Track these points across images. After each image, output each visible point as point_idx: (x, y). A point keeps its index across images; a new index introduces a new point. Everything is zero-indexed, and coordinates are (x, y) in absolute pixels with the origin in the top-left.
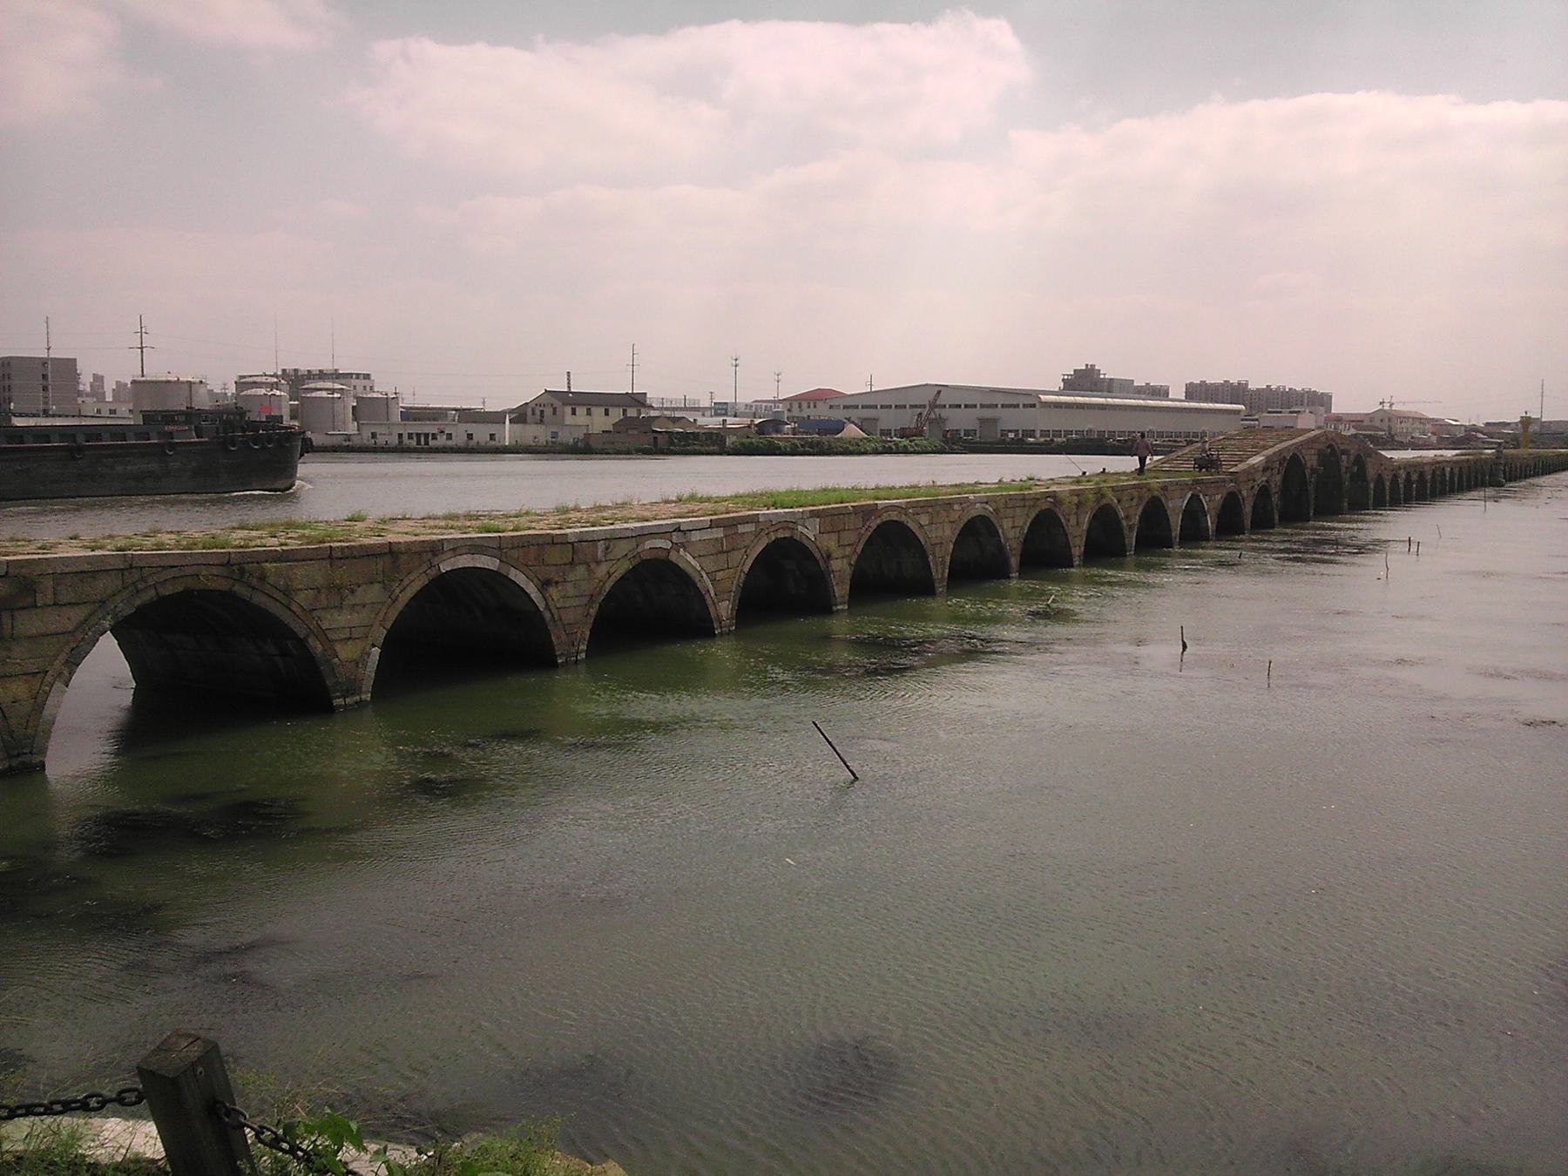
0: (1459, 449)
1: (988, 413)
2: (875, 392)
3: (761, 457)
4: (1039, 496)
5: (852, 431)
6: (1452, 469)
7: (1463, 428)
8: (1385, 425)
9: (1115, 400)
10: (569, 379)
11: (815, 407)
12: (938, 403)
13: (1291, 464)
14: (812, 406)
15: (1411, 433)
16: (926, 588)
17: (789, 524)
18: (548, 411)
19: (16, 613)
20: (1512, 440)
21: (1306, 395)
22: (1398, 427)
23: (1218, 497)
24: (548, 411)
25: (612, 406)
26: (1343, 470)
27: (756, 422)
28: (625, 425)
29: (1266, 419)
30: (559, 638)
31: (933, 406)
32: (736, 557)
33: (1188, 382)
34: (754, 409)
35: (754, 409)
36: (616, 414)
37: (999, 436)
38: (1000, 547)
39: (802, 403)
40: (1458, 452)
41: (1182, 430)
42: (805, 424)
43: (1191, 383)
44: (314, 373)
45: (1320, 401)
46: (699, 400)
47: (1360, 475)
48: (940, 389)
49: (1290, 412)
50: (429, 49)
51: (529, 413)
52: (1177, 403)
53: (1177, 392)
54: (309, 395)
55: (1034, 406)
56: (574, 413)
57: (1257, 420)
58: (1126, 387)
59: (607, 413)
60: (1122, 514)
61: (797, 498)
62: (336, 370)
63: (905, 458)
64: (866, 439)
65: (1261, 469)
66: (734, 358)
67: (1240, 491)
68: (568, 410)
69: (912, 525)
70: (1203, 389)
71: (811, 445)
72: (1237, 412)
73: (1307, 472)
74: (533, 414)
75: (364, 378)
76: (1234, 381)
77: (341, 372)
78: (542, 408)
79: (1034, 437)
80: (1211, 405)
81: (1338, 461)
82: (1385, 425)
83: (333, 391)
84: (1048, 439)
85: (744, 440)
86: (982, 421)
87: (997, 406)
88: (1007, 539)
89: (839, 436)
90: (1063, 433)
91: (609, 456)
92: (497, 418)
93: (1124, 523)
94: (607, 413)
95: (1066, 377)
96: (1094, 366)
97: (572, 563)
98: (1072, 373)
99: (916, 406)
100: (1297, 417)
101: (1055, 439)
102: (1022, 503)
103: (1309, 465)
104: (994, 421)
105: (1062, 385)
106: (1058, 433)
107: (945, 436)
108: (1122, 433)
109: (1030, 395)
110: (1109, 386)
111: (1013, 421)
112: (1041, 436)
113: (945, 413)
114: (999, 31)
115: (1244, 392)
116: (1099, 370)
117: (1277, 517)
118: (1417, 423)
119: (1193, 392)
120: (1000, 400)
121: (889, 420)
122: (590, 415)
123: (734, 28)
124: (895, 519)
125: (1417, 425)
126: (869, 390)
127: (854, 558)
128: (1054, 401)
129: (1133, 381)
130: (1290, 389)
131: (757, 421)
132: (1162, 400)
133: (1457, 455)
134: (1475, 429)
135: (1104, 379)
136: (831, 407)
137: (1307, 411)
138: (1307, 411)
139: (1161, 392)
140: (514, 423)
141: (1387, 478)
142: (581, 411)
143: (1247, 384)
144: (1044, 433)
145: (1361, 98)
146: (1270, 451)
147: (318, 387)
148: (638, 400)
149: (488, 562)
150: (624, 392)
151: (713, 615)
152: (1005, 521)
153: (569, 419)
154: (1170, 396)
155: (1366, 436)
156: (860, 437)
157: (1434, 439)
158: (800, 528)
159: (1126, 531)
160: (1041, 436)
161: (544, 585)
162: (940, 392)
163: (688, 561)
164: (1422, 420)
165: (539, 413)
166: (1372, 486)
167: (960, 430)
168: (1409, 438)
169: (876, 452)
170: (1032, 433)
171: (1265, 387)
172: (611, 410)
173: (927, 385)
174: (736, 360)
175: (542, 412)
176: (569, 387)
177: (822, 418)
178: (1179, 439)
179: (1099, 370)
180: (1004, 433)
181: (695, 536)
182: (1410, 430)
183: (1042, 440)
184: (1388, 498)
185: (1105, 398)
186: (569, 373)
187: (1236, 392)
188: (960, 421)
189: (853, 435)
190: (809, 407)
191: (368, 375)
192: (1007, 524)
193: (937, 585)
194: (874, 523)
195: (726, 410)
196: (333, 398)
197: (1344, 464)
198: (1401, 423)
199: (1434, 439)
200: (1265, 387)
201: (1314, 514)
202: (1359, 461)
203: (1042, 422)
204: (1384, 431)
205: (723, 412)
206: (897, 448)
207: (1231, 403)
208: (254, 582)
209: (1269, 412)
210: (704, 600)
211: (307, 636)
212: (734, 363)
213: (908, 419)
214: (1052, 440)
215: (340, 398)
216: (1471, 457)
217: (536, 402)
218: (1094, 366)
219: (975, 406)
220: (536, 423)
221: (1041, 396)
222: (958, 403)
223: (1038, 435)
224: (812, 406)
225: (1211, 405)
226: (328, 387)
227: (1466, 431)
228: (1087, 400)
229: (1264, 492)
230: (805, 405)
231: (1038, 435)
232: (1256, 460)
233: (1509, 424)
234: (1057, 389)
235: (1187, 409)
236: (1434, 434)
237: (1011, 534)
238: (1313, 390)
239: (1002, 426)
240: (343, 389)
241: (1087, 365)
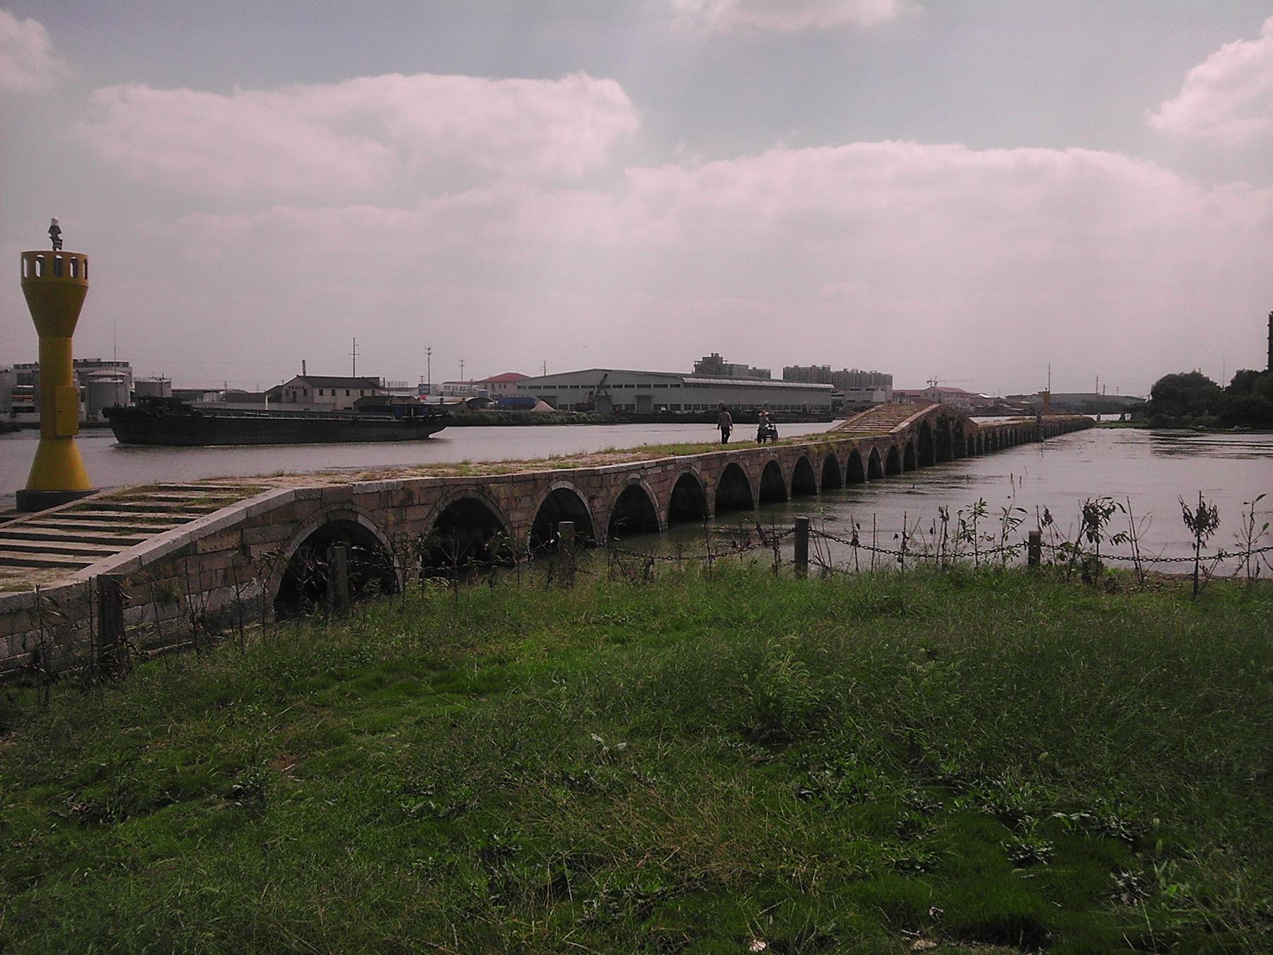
0: (1009, 416)
1: (643, 392)
2: (548, 376)
3: (507, 427)
4: (799, 448)
5: (543, 406)
6: (1011, 430)
7: (992, 400)
9: (739, 381)
10: (304, 367)
11: (505, 387)
12: (605, 384)
13: (922, 427)
14: (502, 387)
15: (955, 404)
16: (749, 507)
17: (688, 465)
18: (300, 393)
19: (407, 509)
20: (1030, 409)
21: (873, 376)
23: (886, 449)
24: (300, 393)
25: (325, 387)
26: (951, 431)
27: (467, 400)
28: (365, 406)
30: (596, 530)
31: (602, 386)
32: (667, 483)
33: (785, 366)
34: (451, 388)
35: (451, 388)
36: (355, 395)
37: (652, 409)
38: (782, 480)
39: (495, 384)
40: (1009, 418)
42: (504, 402)
43: (787, 367)
44: (79, 361)
45: (885, 380)
46: (407, 382)
47: (960, 435)
48: (606, 373)
49: (867, 390)
50: (145, 93)
51: (284, 392)
53: (777, 375)
54: (96, 381)
55: (679, 386)
56: (321, 394)
57: (842, 396)
59: (348, 394)
60: (839, 460)
61: (685, 449)
62: (98, 359)
63: (573, 427)
64: (553, 412)
65: (907, 430)
66: (427, 347)
67: (898, 445)
68: (317, 391)
69: (742, 467)
71: (514, 417)
72: (829, 389)
73: (932, 432)
74: (287, 394)
75: (124, 366)
76: (819, 365)
77: (102, 361)
78: (294, 390)
79: (680, 410)
80: (809, 385)
81: (947, 424)
83: (116, 377)
84: (690, 411)
85: (461, 414)
86: (639, 398)
87: (650, 386)
88: (785, 475)
89: (533, 410)
90: (569, 406)
92: (258, 398)
93: (840, 465)
94: (348, 394)
95: (697, 363)
96: (718, 354)
97: (601, 487)
98: (701, 360)
99: (586, 387)
100: (872, 394)
101: (695, 411)
102: (792, 453)
103: (932, 428)
104: (648, 398)
105: (694, 370)
107: (614, 409)
109: (676, 377)
110: (730, 370)
111: (664, 398)
112: (685, 409)
113: (611, 391)
114: (610, 88)
116: (722, 358)
117: (916, 462)
119: (789, 374)
120: (653, 382)
121: (565, 398)
122: (322, 395)
123: (396, 80)
124: (734, 462)
125: (959, 398)
126: (543, 375)
127: (717, 485)
128: (694, 382)
129: (748, 366)
130: (861, 372)
131: (468, 399)
133: (1008, 420)
134: (999, 400)
135: (726, 364)
136: (519, 387)
137: (880, 389)
138: (880, 389)
139: (765, 375)
140: (273, 402)
141: (975, 436)
142: (327, 392)
143: (829, 368)
144: (688, 407)
145: (888, 146)
146: (911, 419)
147: (102, 374)
148: (372, 383)
149: (569, 485)
150: (361, 377)
151: (658, 519)
152: (784, 463)
153: (317, 399)
154: (772, 378)
156: (550, 411)
157: (972, 409)
158: (693, 467)
159: (841, 471)
160: (685, 409)
161: (591, 499)
162: (606, 375)
163: (647, 485)
164: (963, 395)
165: (292, 393)
166: (967, 442)
167: (567, 406)
169: (562, 423)
170: (678, 407)
171: (842, 370)
172: (351, 391)
173: (594, 370)
174: (429, 349)
175: (294, 392)
176: (304, 373)
177: (517, 396)
179: (722, 358)
180: (658, 407)
181: (650, 472)
182: (954, 402)
183: (686, 412)
184: (976, 450)
186: (304, 361)
187: (822, 374)
188: (623, 398)
189: (543, 409)
190: (500, 387)
191: (127, 363)
192: (785, 465)
193: (754, 504)
194: (725, 464)
195: (429, 390)
196: (117, 383)
197: (951, 427)
198: (948, 397)
199: (972, 409)
200: (842, 370)
201: (937, 461)
202: (959, 425)
203: (685, 398)
205: (426, 391)
206: (579, 419)
208: (486, 494)
209: (851, 390)
210: (654, 510)
211: (505, 525)
212: (427, 351)
213: (581, 397)
214: (693, 412)
215: (121, 383)
216: (1021, 422)
217: (289, 385)
218: (718, 354)
219: (633, 386)
220: (290, 402)
221: (684, 378)
222: (620, 384)
223: (683, 409)
224: (502, 387)
226: (111, 374)
227: (995, 402)
228: (718, 381)
229: (909, 446)
230: (497, 385)
231: (683, 409)
232: (904, 424)
234: (690, 373)
235: (792, 387)
236: (971, 405)
237: (787, 472)
238: (879, 372)
239: (656, 401)
240: (123, 376)
241: (712, 354)
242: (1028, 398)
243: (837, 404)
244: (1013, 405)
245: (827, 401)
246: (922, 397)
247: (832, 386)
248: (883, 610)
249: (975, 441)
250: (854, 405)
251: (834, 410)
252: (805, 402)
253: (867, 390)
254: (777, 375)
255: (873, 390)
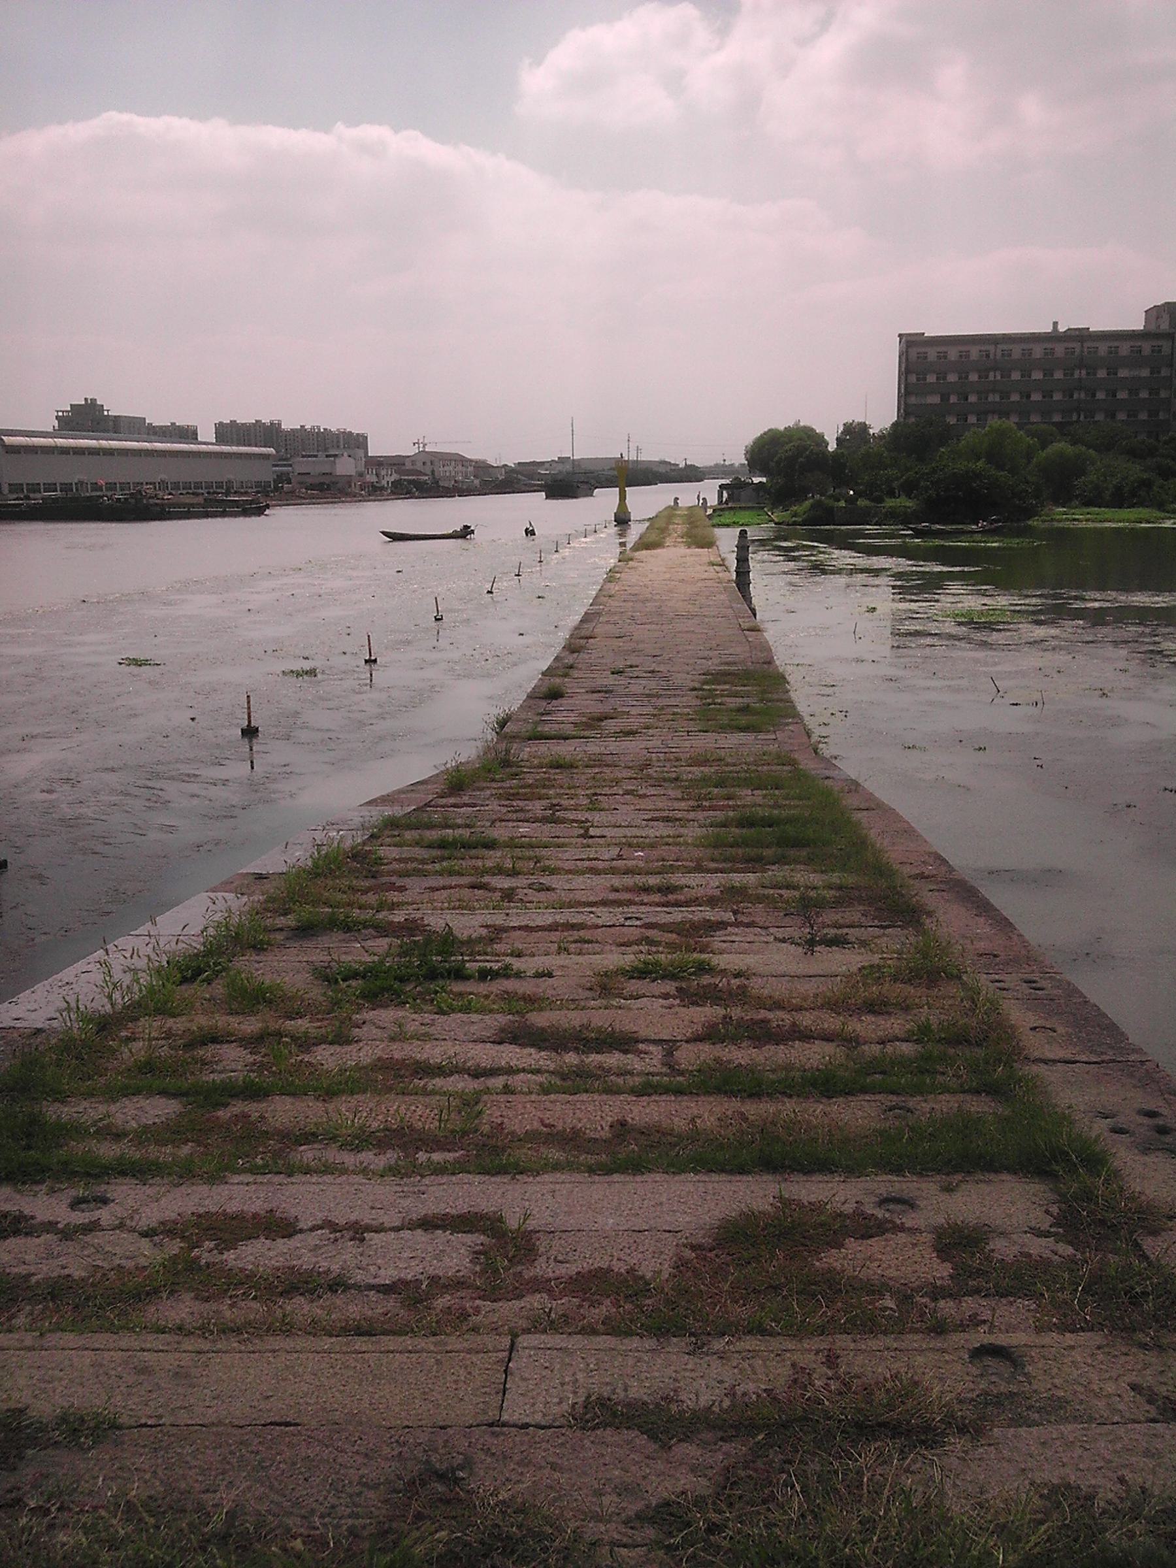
8: (428, 470)
9: (33, 439)
22: (441, 471)
29: (301, 465)
41: (203, 480)
45: (357, 442)
49: (327, 456)
52: (204, 446)
53: (207, 434)
58: (135, 426)
70: (234, 430)
76: (266, 420)
80: (235, 449)
82: (428, 470)
91: (304, 501)
95: (60, 414)
100: (334, 462)
105: (56, 423)
106: (113, 486)
108: (124, 486)
115: (277, 432)
118: (460, 466)
119: (226, 432)
125: (460, 468)
132: (173, 443)
133: (908, 566)
137: (346, 454)
138: (346, 454)
139: (189, 434)
143: (280, 425)
155: (410, 482)
164: (462, 460)
168: (453, 482)
178: (200, 491)
182: (453, 474)
185: (97, 440)
187: (268, 433)
199: (477, 482)
204: (426, 475)
207: (265, 447)
209: (303, 456)
225: (235, 449)
228: (92, 443)
233: (543, 463)
234: (51, 429)
241: (86, 399)
242: (547, 465)
243: (282, 478)
244: (531, 477)
245: (266, 474)
246: (408, 466)
247: (272, 450)
248: (435, 826)
249: (1050, 602)
250: (309, 480)
251: (276, 489)
252: (231, 477)
253: (327, 456)
254: (207, 434)
255: (335, 456)
